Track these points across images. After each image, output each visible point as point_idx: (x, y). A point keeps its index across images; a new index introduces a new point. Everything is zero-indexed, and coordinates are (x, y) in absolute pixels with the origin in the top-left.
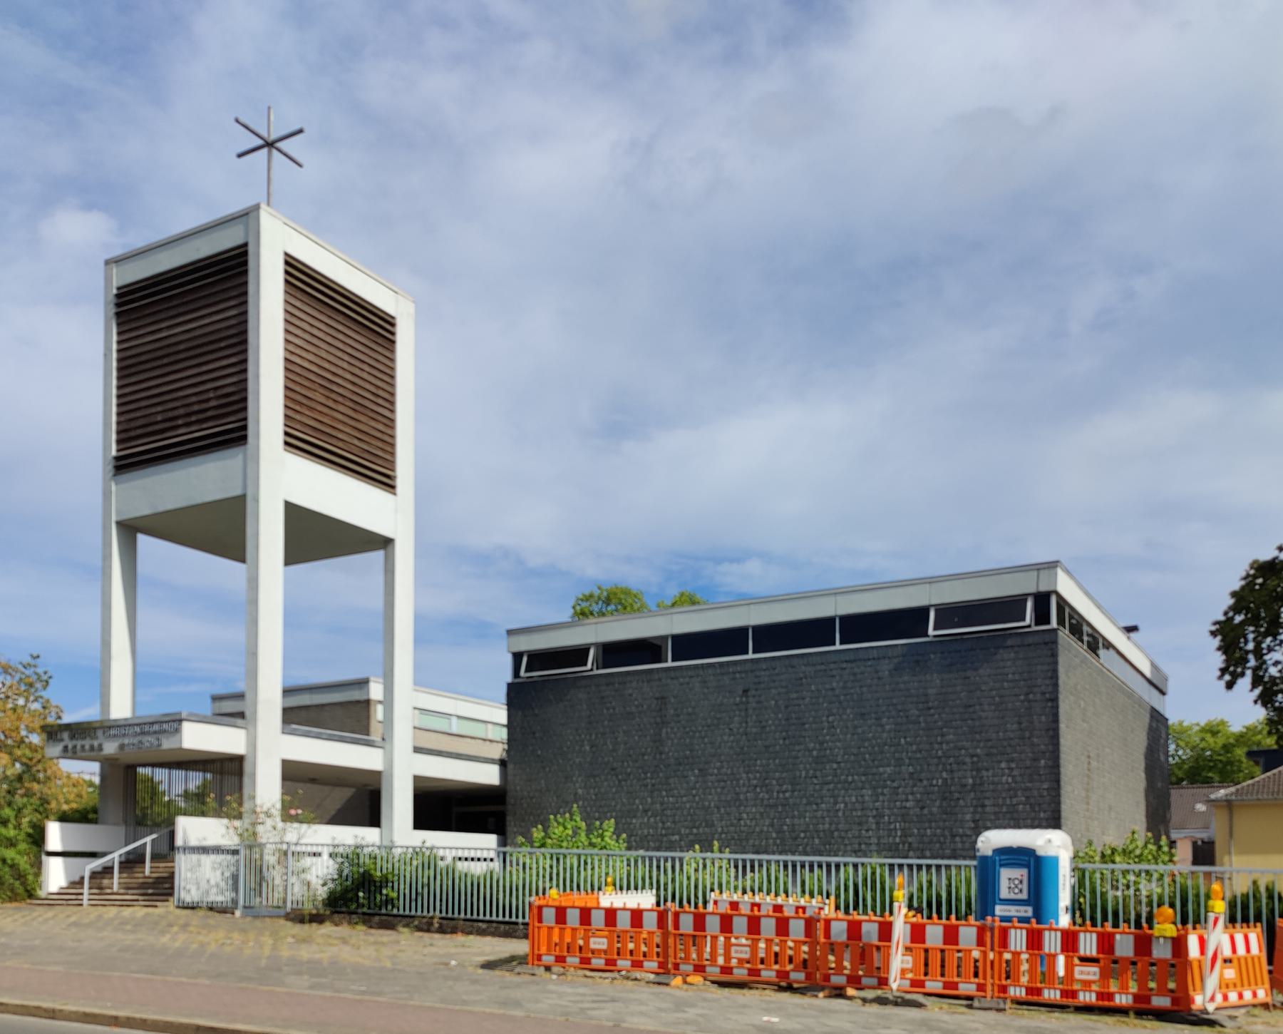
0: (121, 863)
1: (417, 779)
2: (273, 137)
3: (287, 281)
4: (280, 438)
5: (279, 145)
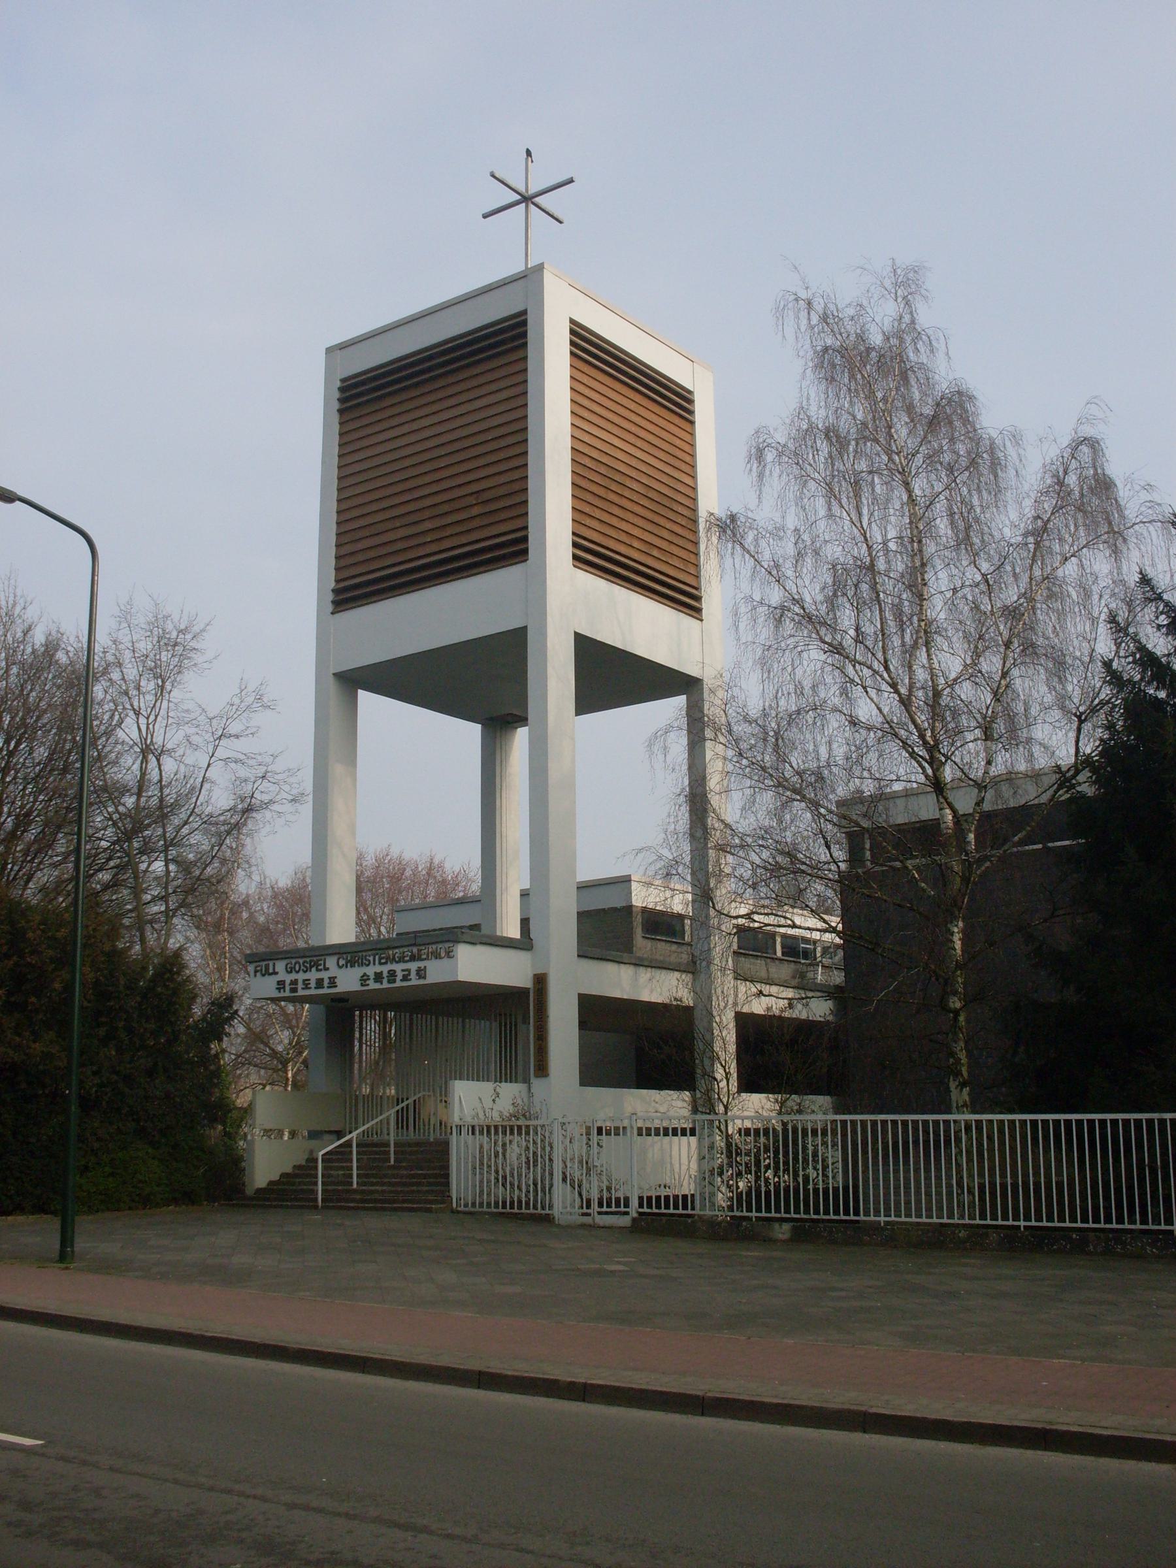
2: (532, 190)
3: (572, 353)
4: (567, 550)
5: (537, 200)
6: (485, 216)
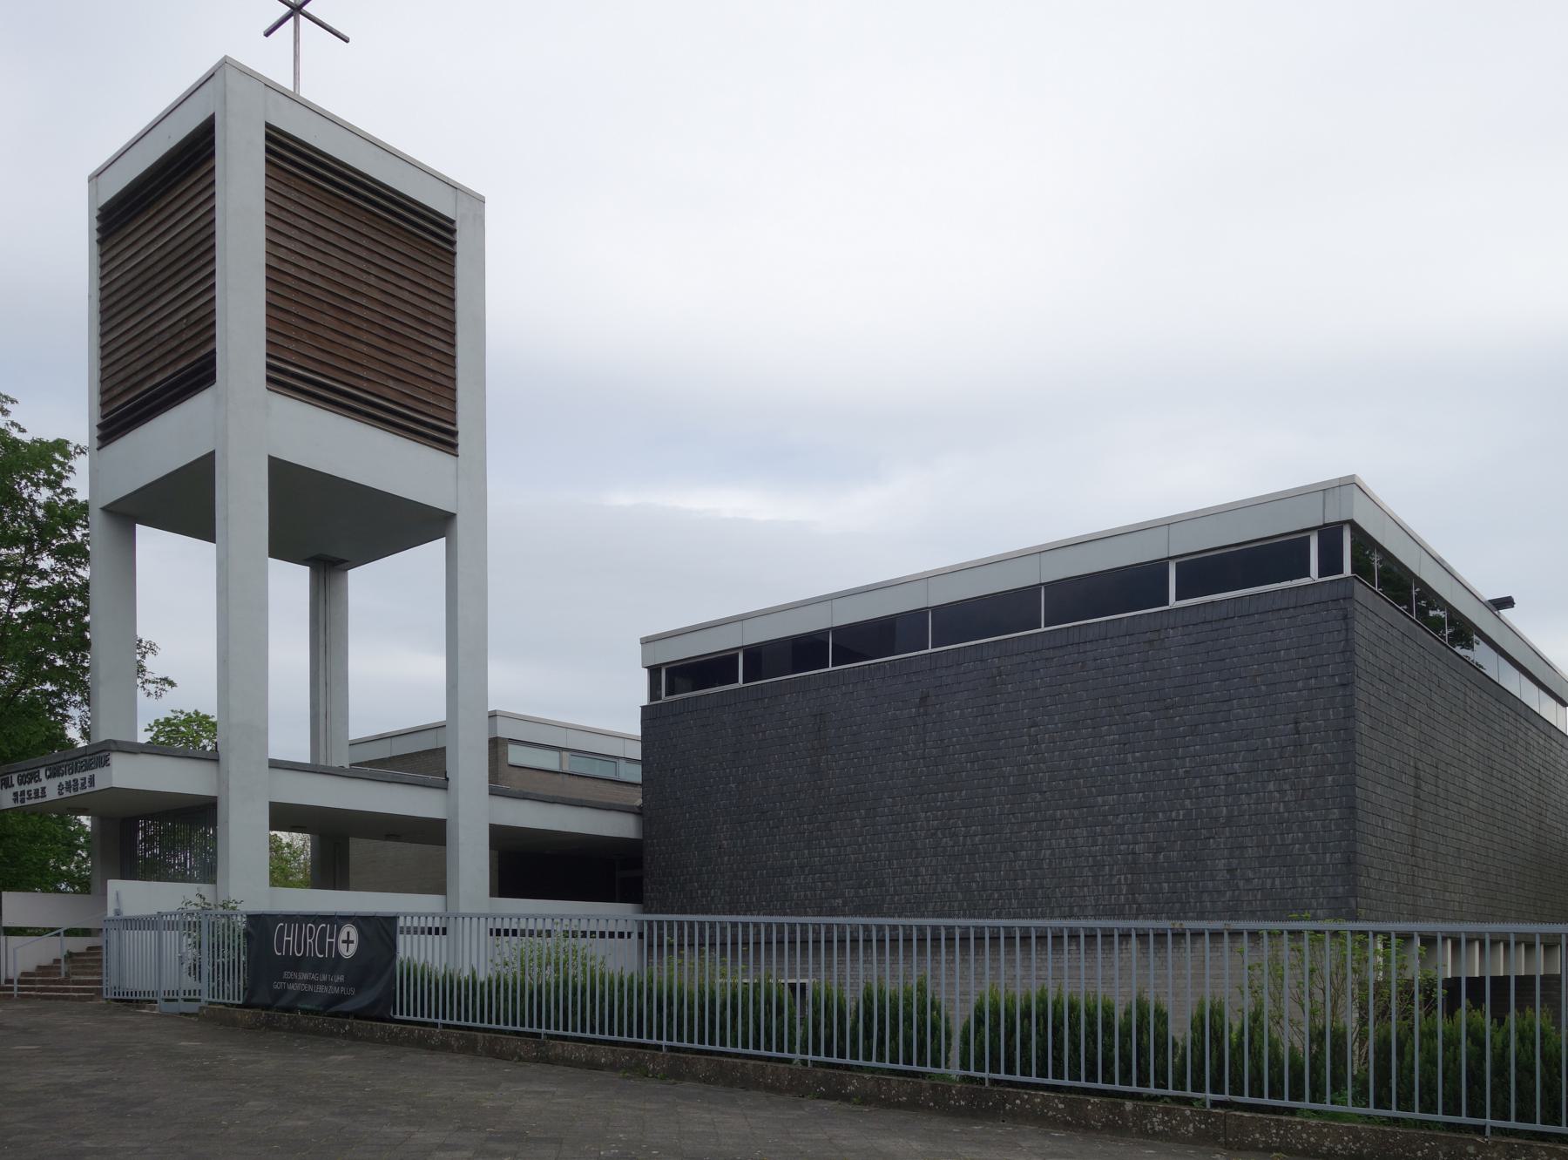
0: (645, 912)
1: (494, 829)
3: (267, 161)
6: (267, 34)
